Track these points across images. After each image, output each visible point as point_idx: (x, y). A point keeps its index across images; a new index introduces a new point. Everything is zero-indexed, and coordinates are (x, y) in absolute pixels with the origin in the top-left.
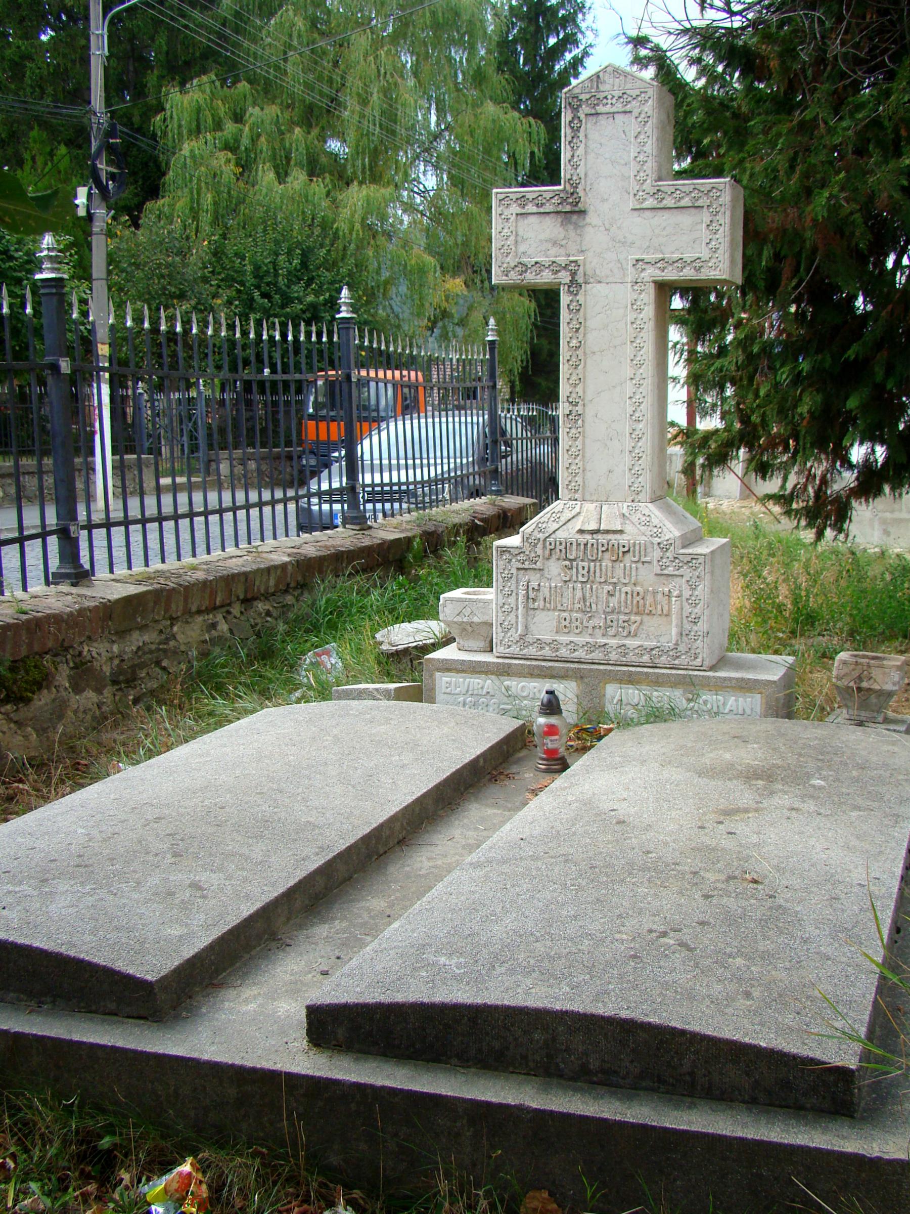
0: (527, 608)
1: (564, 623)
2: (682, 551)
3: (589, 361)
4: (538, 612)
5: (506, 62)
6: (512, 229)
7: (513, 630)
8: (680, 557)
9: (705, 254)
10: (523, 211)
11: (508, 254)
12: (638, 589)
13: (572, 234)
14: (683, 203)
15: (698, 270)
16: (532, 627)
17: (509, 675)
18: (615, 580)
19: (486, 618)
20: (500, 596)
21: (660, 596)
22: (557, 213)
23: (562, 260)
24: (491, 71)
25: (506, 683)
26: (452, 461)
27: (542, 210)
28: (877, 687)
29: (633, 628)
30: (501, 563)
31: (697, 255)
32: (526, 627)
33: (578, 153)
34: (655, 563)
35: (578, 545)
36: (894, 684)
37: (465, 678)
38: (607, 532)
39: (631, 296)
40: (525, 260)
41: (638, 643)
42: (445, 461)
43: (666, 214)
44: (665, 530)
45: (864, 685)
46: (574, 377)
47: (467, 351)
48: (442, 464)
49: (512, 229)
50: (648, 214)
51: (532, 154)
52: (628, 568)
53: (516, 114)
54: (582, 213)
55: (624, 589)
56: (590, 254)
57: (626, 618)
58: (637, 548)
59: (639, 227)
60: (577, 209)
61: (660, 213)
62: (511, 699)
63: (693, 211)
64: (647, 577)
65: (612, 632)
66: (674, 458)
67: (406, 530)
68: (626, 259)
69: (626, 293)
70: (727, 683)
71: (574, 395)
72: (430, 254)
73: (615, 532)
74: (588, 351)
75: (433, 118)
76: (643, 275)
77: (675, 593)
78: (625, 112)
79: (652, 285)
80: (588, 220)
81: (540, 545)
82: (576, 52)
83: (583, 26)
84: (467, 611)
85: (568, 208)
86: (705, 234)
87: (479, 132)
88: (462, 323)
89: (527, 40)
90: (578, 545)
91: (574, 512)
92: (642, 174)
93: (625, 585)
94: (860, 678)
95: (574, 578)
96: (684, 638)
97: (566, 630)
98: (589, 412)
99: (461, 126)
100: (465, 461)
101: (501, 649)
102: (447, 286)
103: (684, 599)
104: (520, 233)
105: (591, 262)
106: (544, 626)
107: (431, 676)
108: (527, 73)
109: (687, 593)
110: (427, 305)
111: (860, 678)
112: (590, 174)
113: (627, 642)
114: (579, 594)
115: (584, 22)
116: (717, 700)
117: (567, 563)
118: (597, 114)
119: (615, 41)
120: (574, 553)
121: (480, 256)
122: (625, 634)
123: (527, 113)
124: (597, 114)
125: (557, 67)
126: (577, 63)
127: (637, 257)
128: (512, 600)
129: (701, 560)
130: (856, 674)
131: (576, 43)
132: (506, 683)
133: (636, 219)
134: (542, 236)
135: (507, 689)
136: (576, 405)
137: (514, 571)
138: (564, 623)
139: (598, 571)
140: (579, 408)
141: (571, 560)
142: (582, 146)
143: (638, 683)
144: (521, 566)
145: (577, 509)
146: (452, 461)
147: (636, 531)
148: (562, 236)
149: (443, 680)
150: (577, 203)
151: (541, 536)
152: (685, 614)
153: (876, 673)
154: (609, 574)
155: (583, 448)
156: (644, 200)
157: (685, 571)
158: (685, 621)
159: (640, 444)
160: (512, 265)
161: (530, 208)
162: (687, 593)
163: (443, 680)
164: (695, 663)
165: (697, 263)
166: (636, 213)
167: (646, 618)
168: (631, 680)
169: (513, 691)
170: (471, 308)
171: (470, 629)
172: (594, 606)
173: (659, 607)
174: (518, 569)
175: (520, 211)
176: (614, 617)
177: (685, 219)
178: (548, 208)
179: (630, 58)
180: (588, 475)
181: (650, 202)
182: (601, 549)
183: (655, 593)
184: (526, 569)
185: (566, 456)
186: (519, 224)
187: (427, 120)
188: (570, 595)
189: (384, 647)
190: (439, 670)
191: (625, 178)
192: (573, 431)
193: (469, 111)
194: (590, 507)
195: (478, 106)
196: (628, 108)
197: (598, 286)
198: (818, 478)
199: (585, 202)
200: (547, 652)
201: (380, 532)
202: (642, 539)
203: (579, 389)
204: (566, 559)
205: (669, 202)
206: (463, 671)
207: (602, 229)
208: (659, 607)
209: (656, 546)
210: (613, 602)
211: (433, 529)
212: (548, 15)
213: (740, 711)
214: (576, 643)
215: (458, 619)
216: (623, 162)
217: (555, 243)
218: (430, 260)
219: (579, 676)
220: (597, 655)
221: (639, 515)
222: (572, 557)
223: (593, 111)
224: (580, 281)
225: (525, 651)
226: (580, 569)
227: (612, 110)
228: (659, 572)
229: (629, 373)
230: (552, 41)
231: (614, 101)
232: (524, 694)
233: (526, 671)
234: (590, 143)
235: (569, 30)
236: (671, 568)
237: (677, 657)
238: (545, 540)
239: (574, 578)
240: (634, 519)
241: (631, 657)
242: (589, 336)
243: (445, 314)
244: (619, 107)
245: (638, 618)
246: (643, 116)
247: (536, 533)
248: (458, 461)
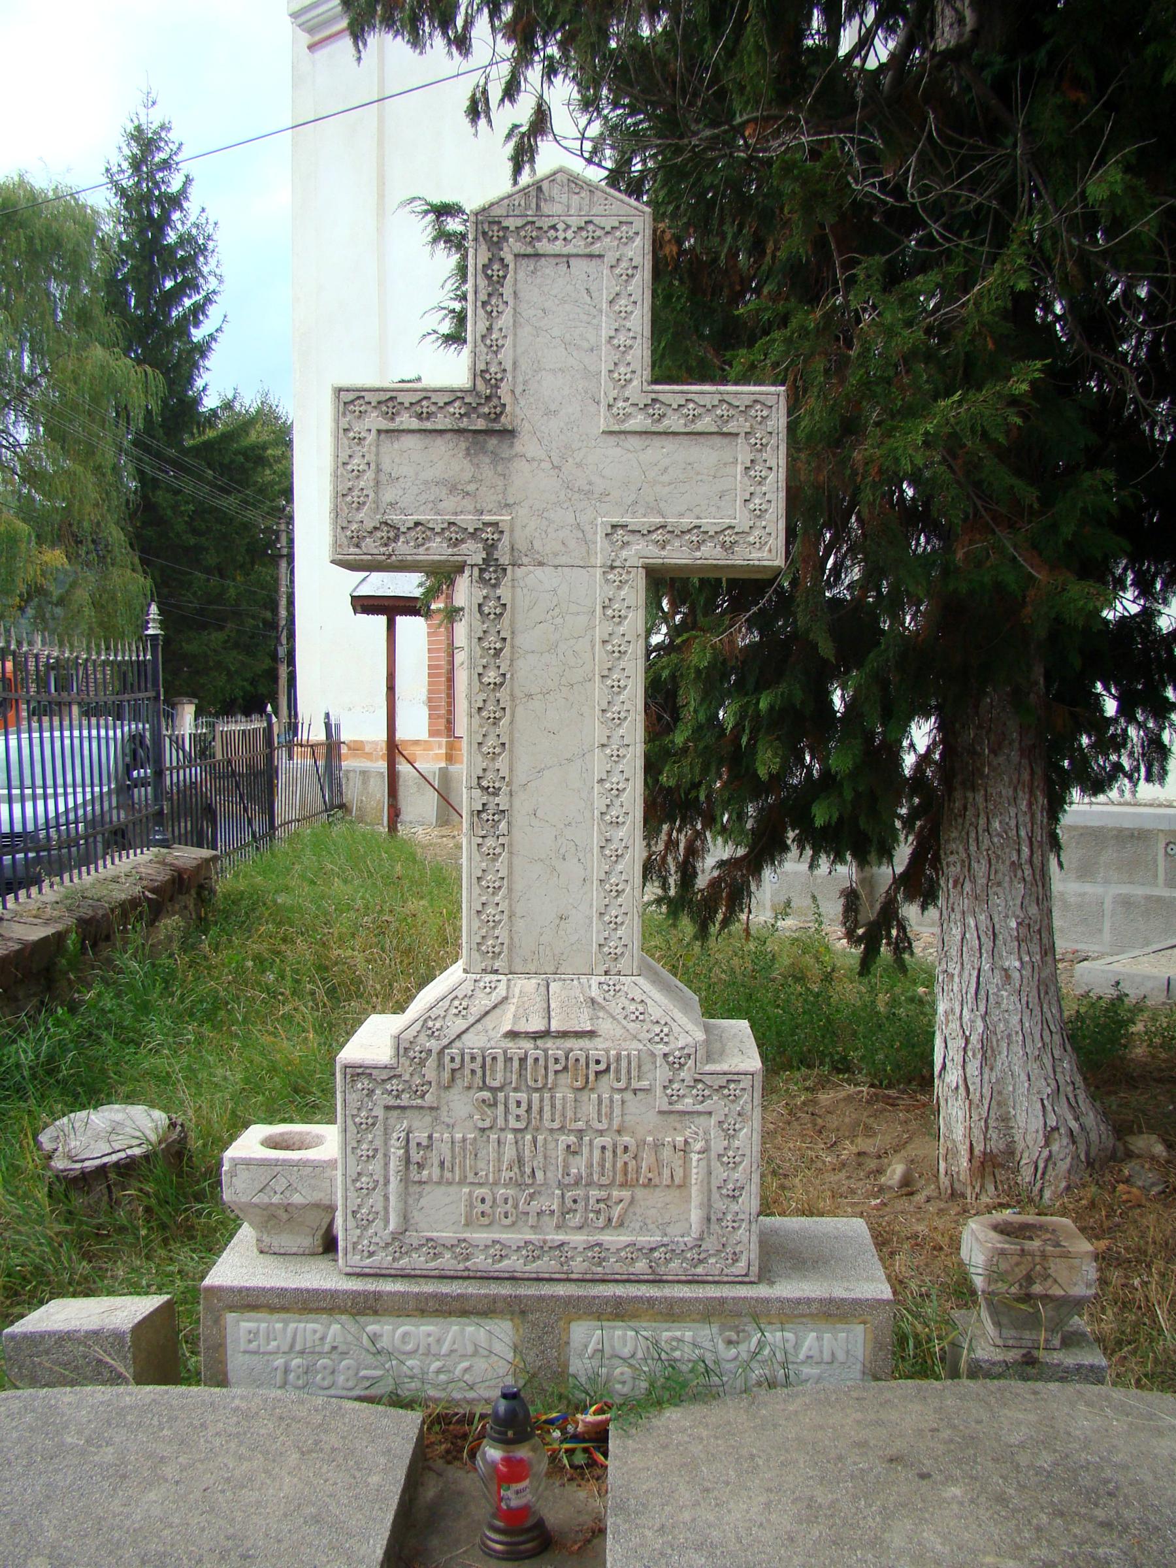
0: (405, 1181)
1: (481, 1207)
2: (709, 1068)
3: (520, 710)
4: (428, 1188)
5: (116, 303)
6: (370, 457)
7: (378, 1224)
8: (706, 1078)
9: (742, 520)
10: (392, 426)
11: (361, 505)
12: (626, 1139)
13: (487, 472)
14: (699, 426)
15: (728, 548)
16: (416, 1216)
17: (376, 1313)
18: (580, 1125)
19: (317, 1196)
20: (352, 1160)
21: (666, 1153)
22: (460, 431)
23: (468, 520)
24: (97, 311)
25: (370, 1328)
26: (88, 789)
27: (428, 425)
28: (1057, 1291)
29: (617, 1211)
30: (353, 1097)
31: (728, 521)
32: (405, 1217)
33: (500, 323)
34: (659, 1090)
35: (508, 1060)
36: (1088, 1286)
37: (286, 1323)
38: (564, 1034)
39: (601, 592)
40: (394, 517)
41: (625, 1239)
42: (79, 790)
43: (670, 444)
44: (676, 1029)
45: (1037, 1289)
46: (491, 741)
47: (108, 648)
48: (75, 793)
49: (370, 457)
50: (634, 441)
51: (149, 412)
52: (606, 1102)
53: (129, 362)
54: (509, 434)
55: (599, 1141)
56: (522, 512)
57: (603, 1194)
58: (624, 1064)
59: (618, 465)
60: (497, 427)
61: (657, 442)
62: (382, 1359)
63: (718, 440)
64: (642, 1116)
65: (576, 1220)
66: (351, 775)
67: (56, 920)
68: (592, 523)
69: (591, 587)
70: (803, 1308)
71: (490, 775)
72: (24, 520)
73: (579, 1035)
74: (518, 693)
75: (27, 361)
76: (624, 553)
77: (698, 1146)
78: (591, 256)
79: (642, 572)
80: (518, 447)
81: (431, 1062)
82: (196, 298)
83: (205, 270)
84: (280, 1184)
85: (481, 424)
86: (740, 483)
87: (85, 380)
88: (61, 602)
89: (140, 281)
90: (508, 1060)
91: (495, 997)
92: (622, 370)
93: (601, 1133)
94: (1029, 1279)
95: (500, 1122)
96: (715, 1227)
97: (485, 1221)
98: (522, 807)
99: (63, 371)
100: (105, 789)
101: (355, 1259)
102: (45, 558)
103: (713, 1155)
104: (386, 466)
105: (524, 527)
106: (442, 1215)
107: (217, 1321)
108: (139, 318)
109: (718, 1145)
110: (19, 581)
111: (1029, 1279)
112: (523, 365)
113: (607, 1238)
114: (509, 1153)
115: (206, 267)
116: (784, 1340)
117: (486, 1094)
118: (537, 255)
119: (408, 208)
120: (499, 1076)
121: (86, 524)
122: (601, 1222)
123: (139, 361)
124: (537, 255)
125: (174, 314)
126: (199, 310)
127: (615, 520)
128: (375, 1166)
129: (746, 1083)
130: (1021, 1272)
131: (197, 288)
132: (370, 1328)
133: (612, 450)
134: (428, 474)
135: (373, 1339)
136: (496, 793)
137: (379, 1112)
138: (481, 1207)
139: (547, 1108)
140: (502, 800)
141: (494, 1090)
142: (509, 310)
143: (635, 1316)
144: (392, 1102)
145: (501, 991)
146: (88, 789)
147: (619, 1032)
148: (467, 476)
149: (241, 1329)
150: (498, 416)
151: (434, 1045)
152: (715, 1183)
153: (1057, 1268)
154: (570, 1114)
155: (510, 873)
156: (628, 416)
157: (715, 1102)
158: (715, 1195)
159: (620, 867)
160: (369, 525)
161: (406, 420)
162: (718, 1145)
163: (241, 1329)
164: (733, 1270)
165: (728, 537)
166: (612, 440)
167: (640, 1193)
168: (619, 1311)
169: (383, 1343)
170: (74, 585)
171: (285, 1216)
172: (539, 1175)
173: (666, 1172)
174: (388, 1108)
175: (385, 424)
176: (579, 1192)
177: (706, 455)
178: (441, 421)
179: (430, 233)
180: (520, 924)
181: (638, 421)
182: (552, 1067)
183: (658, 1146)
184: (403, 1108)
185: (476, 890)
186: (383, 450)
187: (19, 360)
188: (493, 1156)
189: (59, 1164)
190: (232, 1308)
191: (591, 375)
192: (490, 842)
193: (73, 354)
194: (526, 986)
195: (84, 350)
196: (596, 248)
197: (539, 571)
198: (682, 846)
199: (513, 415)
200: (447, 1261)
201: (16, 926)
202: (633, 1048)
203: (502, 763)
204: (484, 1087)
205: (674, 422)
206: (284, 1309)
207: (546, 465)
208: (666, 1172)
209: (660, 1060)
210: (578, 1166)
211: (91, 913)
212: (165, 254)
213: (827, 1356)
214: (504, 1243)
215: (262, 1199)
216: (586, 345)
217: (453, 489)
218: (23, 527)
219: (517, 1309)
220: (546, 1265)
221: (623, 1001)
222: (496, 1084)
223: (530, 250)
224: (505, 560)
225: (403, 1262)
226: (512, 1105)
227: (565, 251)
228: (666, 1107)
229: (599, 733)
230: (169, 284)
231: (569, 234)
232: (409, 1347)
233: (412, 1304)
234: (523, 307)
235: (188, 274)
236: (689, 1100)
237: (700, 1261)
238: (441, 1052)
239: (500, 1122)
240: (615, 1007)
241: (612, 1265)
242: (520, 663)
243: (40, 591)
244: (578, 245)
245: (626, 1194)
246: (624, 264)
247: (422, 1039)
248: (97, 789)
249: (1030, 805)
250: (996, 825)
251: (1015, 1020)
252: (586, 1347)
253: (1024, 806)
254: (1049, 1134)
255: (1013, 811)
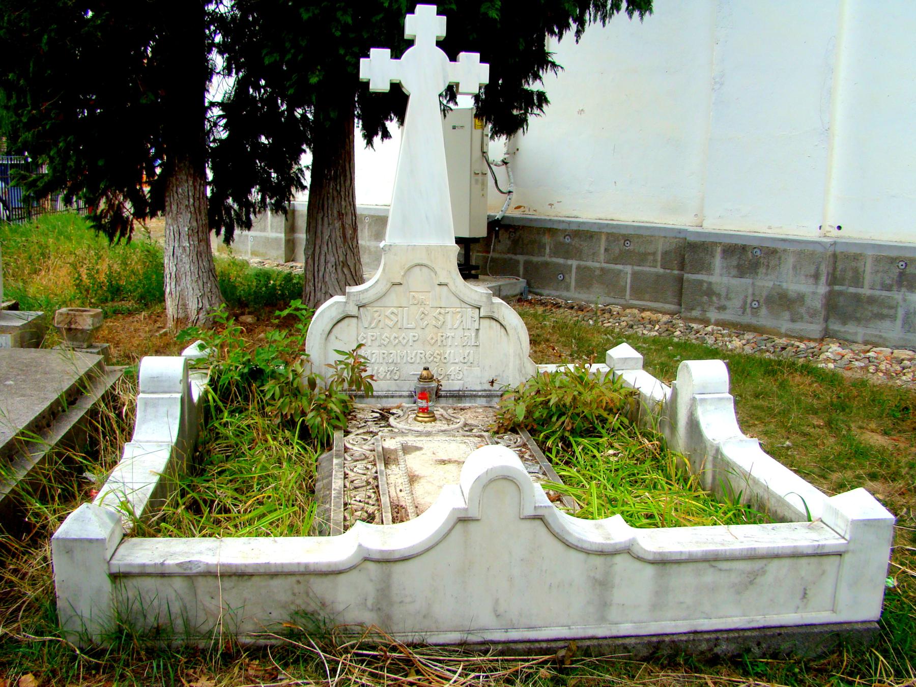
45: (73, 326)
94: (70, 323)
111: (70, 323)
130: (68, 320)
249: (194, 183)
250: (180, 190)
251: (188, 266)
252: (439, 631)
253: (191, 183)
254: (199, 310)
255: (186, 185)
